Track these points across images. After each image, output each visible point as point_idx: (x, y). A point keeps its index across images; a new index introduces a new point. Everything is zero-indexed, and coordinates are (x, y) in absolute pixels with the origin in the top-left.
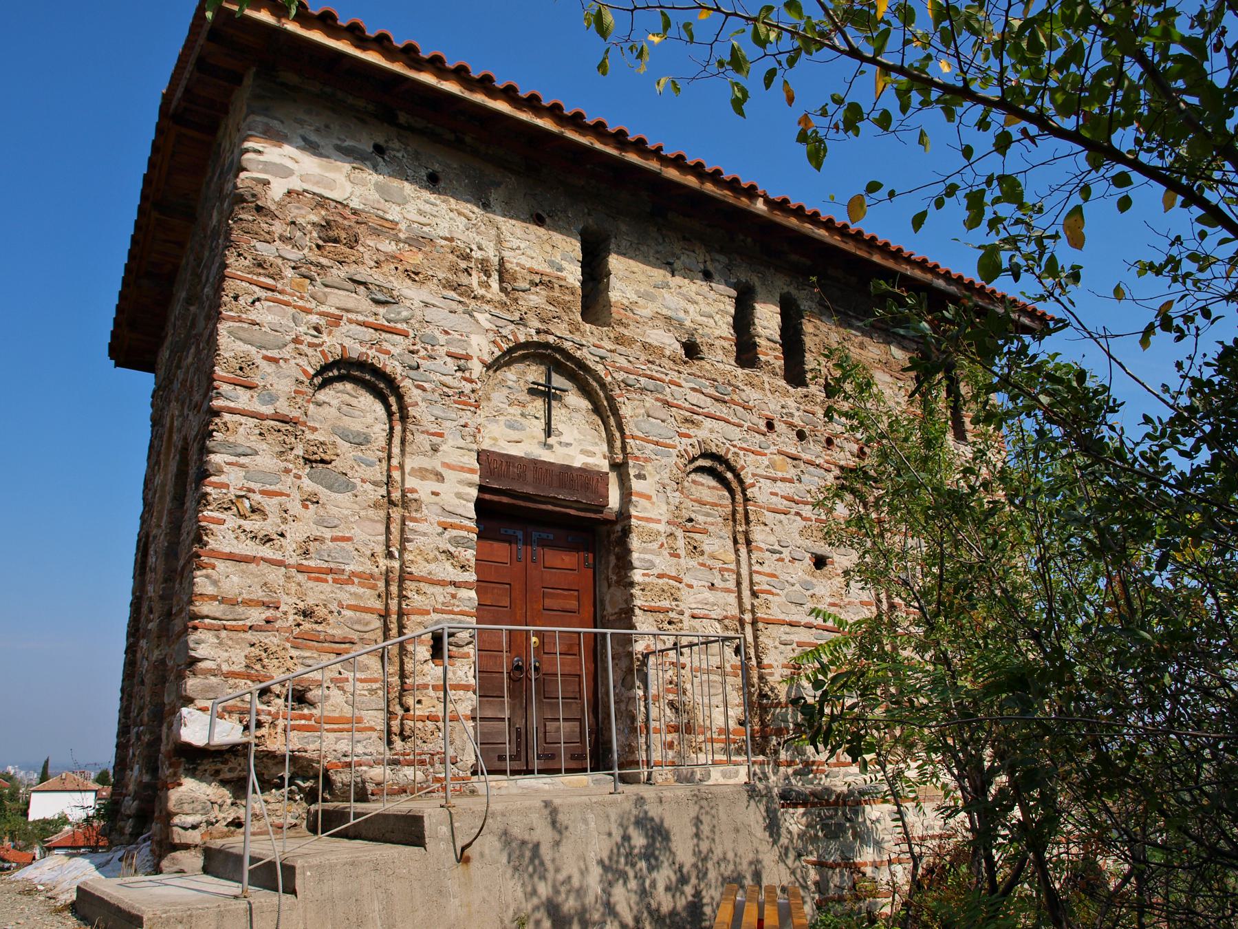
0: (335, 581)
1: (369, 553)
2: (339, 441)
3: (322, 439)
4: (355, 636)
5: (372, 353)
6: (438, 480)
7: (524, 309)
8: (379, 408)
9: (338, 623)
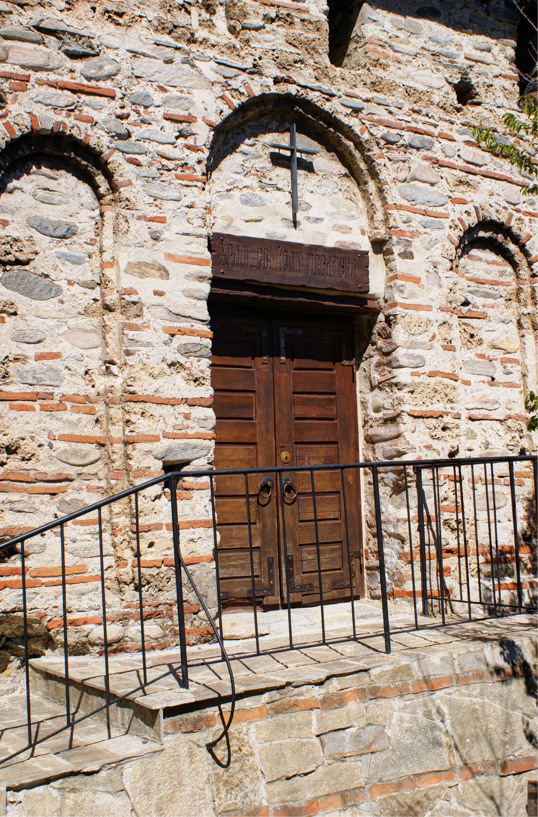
0: (43, 408)
1: (82, 371)
2: (37, 236)
3: (15, 235)
4: (72, 471)
5: (70, 121)
6: (161, 276)
7: (258, 53)
8: (84, 188)
9: (51, 458)
